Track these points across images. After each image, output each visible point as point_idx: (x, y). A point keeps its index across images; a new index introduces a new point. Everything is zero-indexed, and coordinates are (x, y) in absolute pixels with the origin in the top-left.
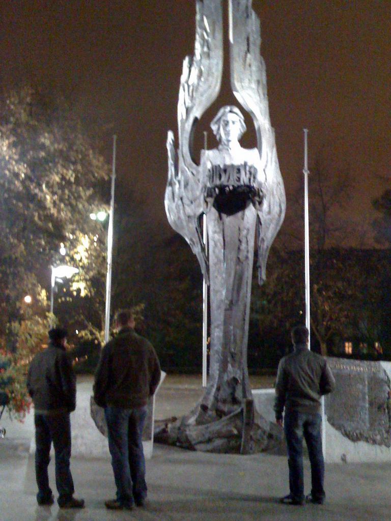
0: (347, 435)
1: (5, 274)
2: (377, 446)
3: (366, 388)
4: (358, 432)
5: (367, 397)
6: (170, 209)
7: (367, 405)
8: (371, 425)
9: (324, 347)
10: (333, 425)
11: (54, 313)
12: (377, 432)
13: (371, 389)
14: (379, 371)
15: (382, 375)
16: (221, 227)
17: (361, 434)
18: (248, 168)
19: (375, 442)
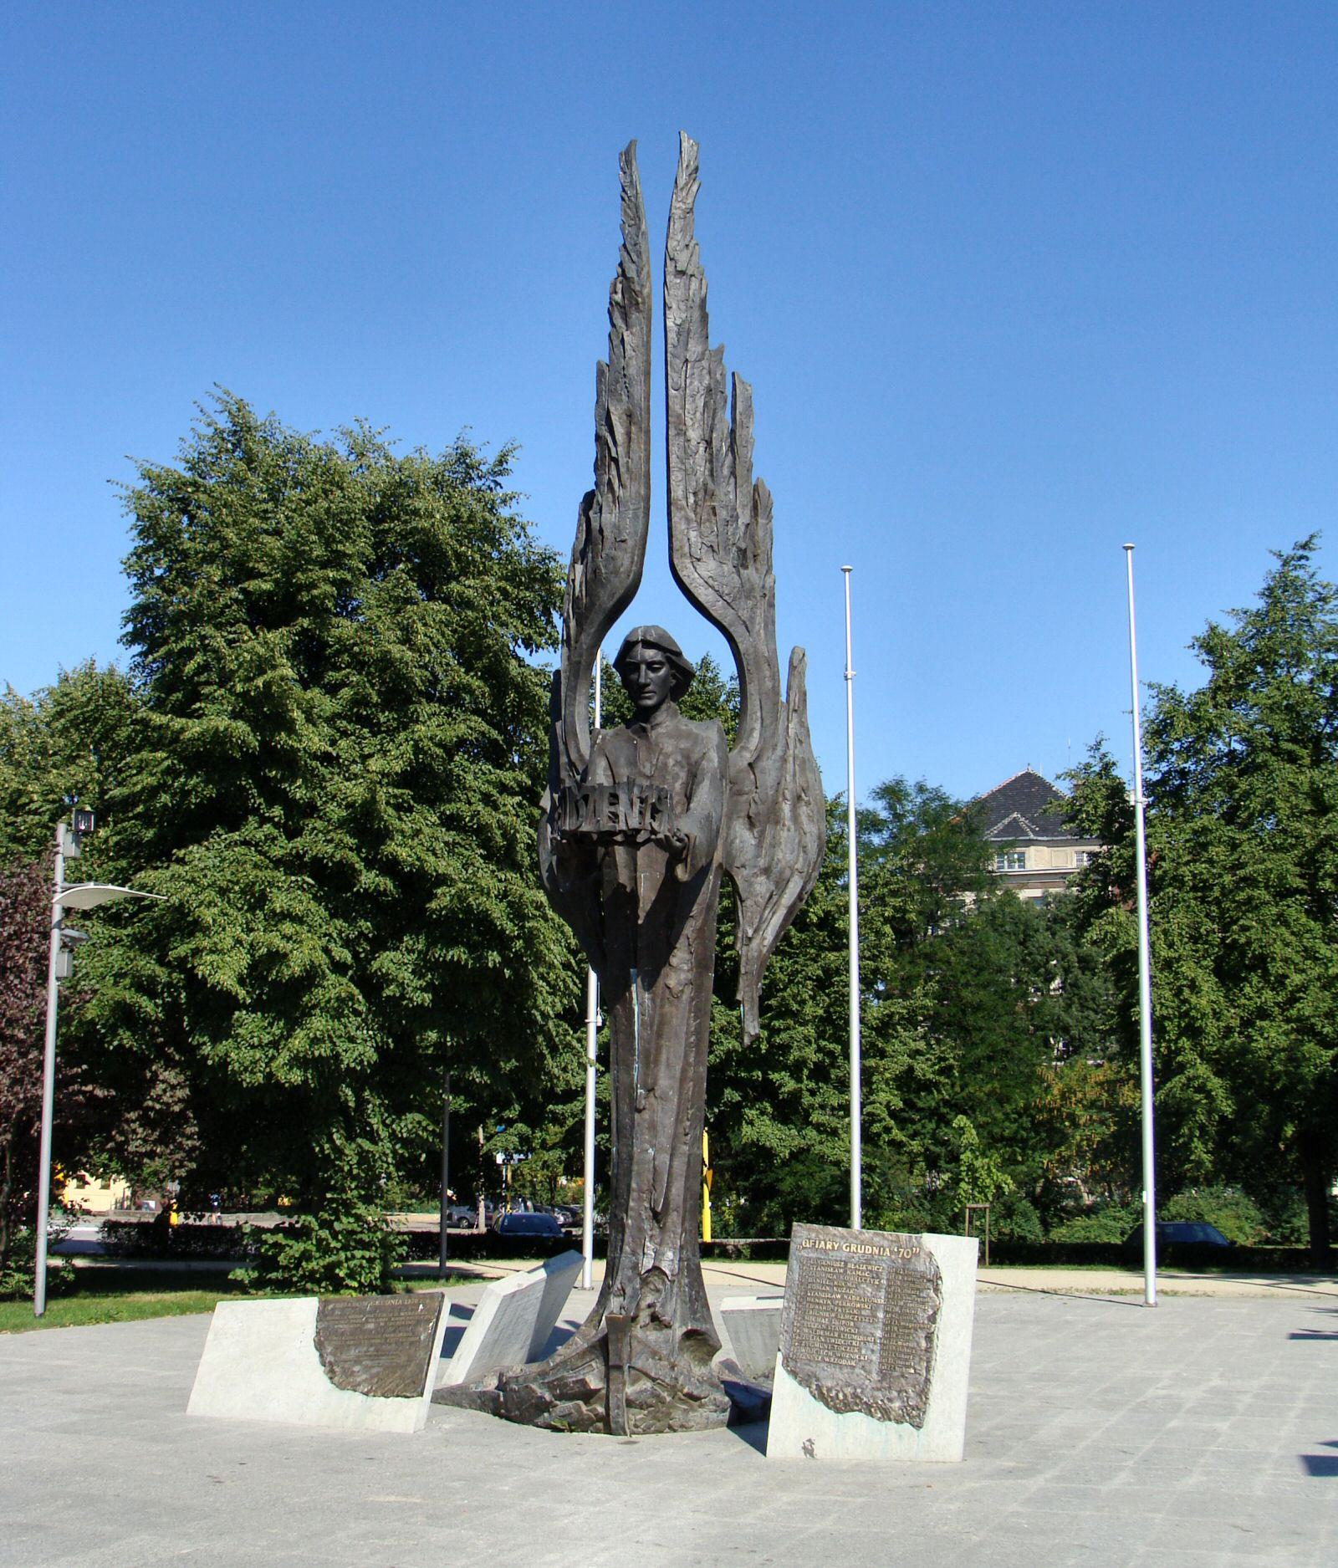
0: (822, 1396)
1: (1334, 1067)
2: (892, 1424)
3: (882, 1294)
4: (849, 1391)
5: (881, 1315)
6: (597, 618)
7: (879, 1334)
8: (883, 1375)
9: (981, 1297)
10: (794, 1373)
11: (418, 803)
12: (895, 1394)
13: (891, 1296)
14: (917, 1255)
15: (921, 1266)
16: (732, 832)
17: (855, 1395)
18: (1306, 553)
19: (886, 1415)
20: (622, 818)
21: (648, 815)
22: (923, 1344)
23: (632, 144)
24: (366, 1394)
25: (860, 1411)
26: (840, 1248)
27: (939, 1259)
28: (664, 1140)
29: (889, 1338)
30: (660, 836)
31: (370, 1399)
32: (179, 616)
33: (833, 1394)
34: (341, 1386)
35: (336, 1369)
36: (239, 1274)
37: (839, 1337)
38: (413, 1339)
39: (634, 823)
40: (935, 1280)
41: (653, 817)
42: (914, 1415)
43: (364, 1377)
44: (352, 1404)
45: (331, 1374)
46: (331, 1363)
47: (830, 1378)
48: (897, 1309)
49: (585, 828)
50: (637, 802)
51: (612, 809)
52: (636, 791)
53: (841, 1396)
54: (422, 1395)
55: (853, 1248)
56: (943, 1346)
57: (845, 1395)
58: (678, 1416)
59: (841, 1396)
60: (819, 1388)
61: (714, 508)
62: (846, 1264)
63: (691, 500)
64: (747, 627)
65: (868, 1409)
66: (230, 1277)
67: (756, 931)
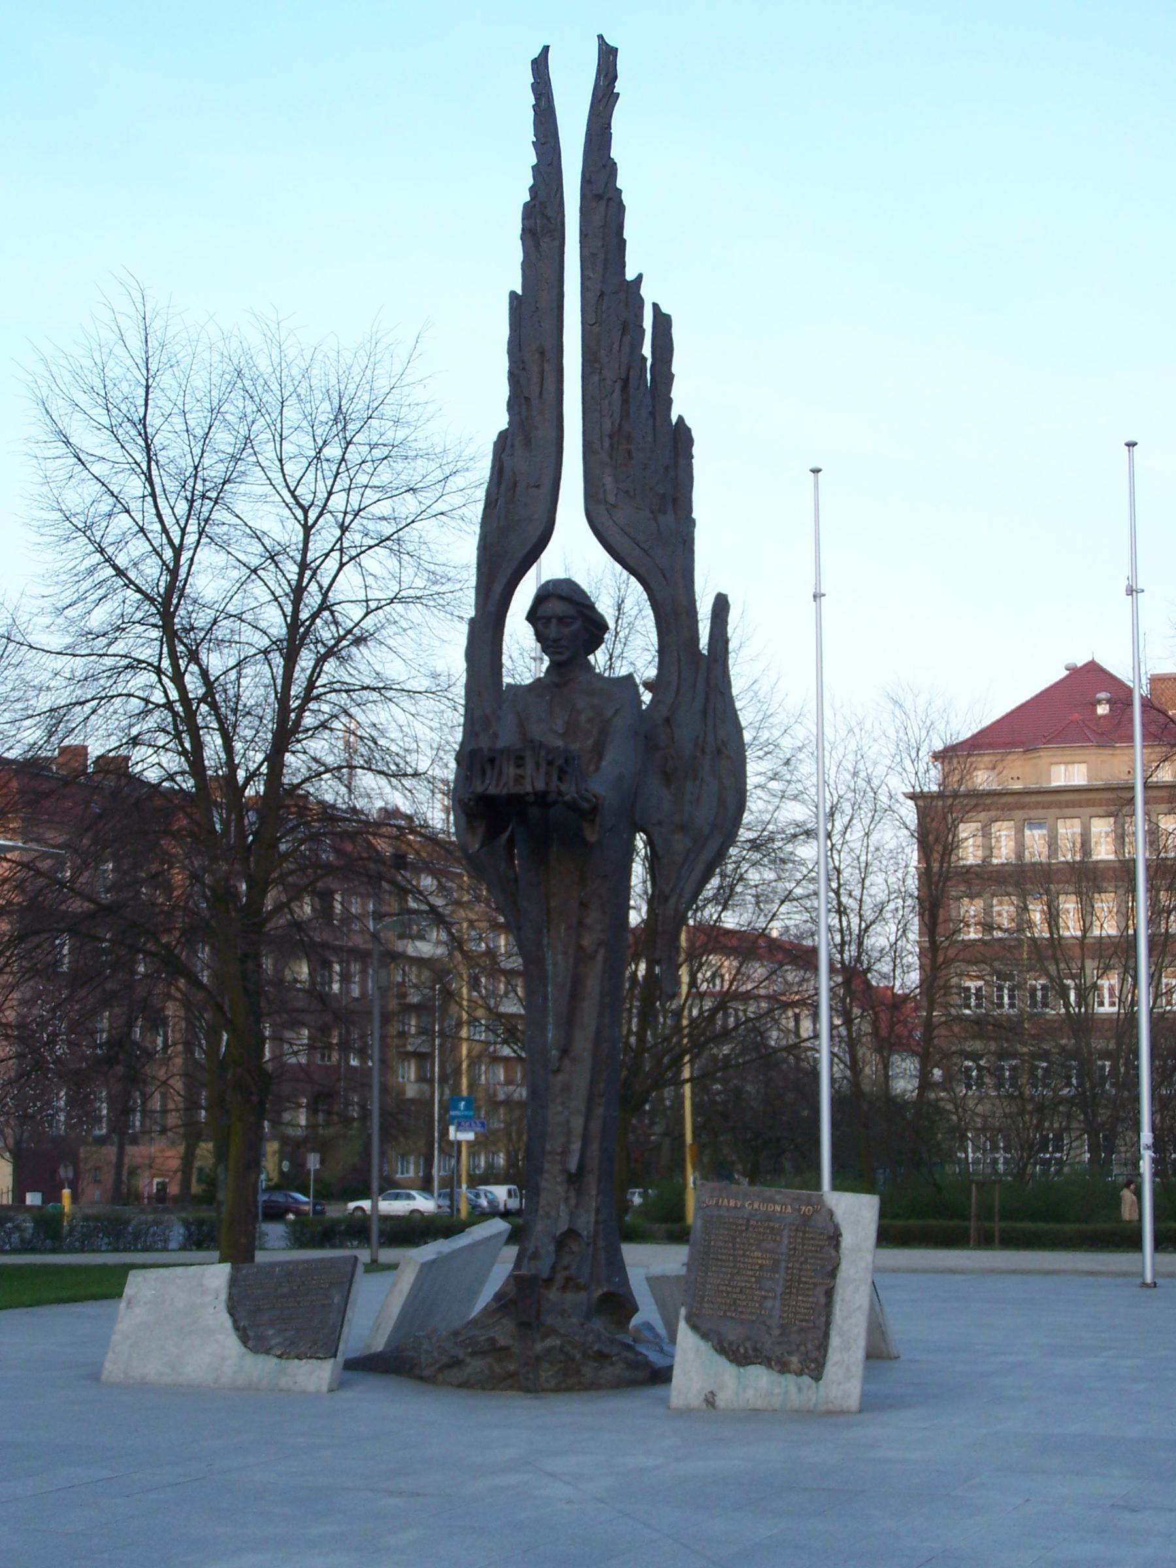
2: (791, 1378)
10: (695, 1327)
20: (528, 780)
21: (555, 778)
22: (823, 1300)
23: (546, 49)
24: (280, 1357)
25: (760, 1364)
26: (743, 1206)
27: (840, 1216)
28: (579, 1103)
29: (790, 1293)
30: (567, 798)
31: (283, 1361)
32: (128, 1096)
33: (734, 1348)
34: (255, 1350)
35: (251, 1334)
36: (1131, 932)
37: (741, 1292)
38: (326, 1302)
39: (540, 785)
40: (835, 1238)
41: (560, 779)
42: (815, 1366)
43: (278, 1340)
44: (262, 1367)
45: (244, 1339)
46: (245, 1329)
47: (733, 1333)
48: (797, 1265)
49: (492, 791)
50: (543, 765)
51: (519, 771)
52: (543, 753)
53: (742, 1351)
54: (335, 1356)
55: (756, 1205)
56: (842, 1300)
57: (746, 1349)
58: (588, 1371)
59: (742, 1351)
60: (720, 1342)
61: (629, 452)
62: (748, 1221)
63: (606, 444)
64: (664, 576)
65: (767, 1362)
66: (644, 707)
67: (672, 890)
